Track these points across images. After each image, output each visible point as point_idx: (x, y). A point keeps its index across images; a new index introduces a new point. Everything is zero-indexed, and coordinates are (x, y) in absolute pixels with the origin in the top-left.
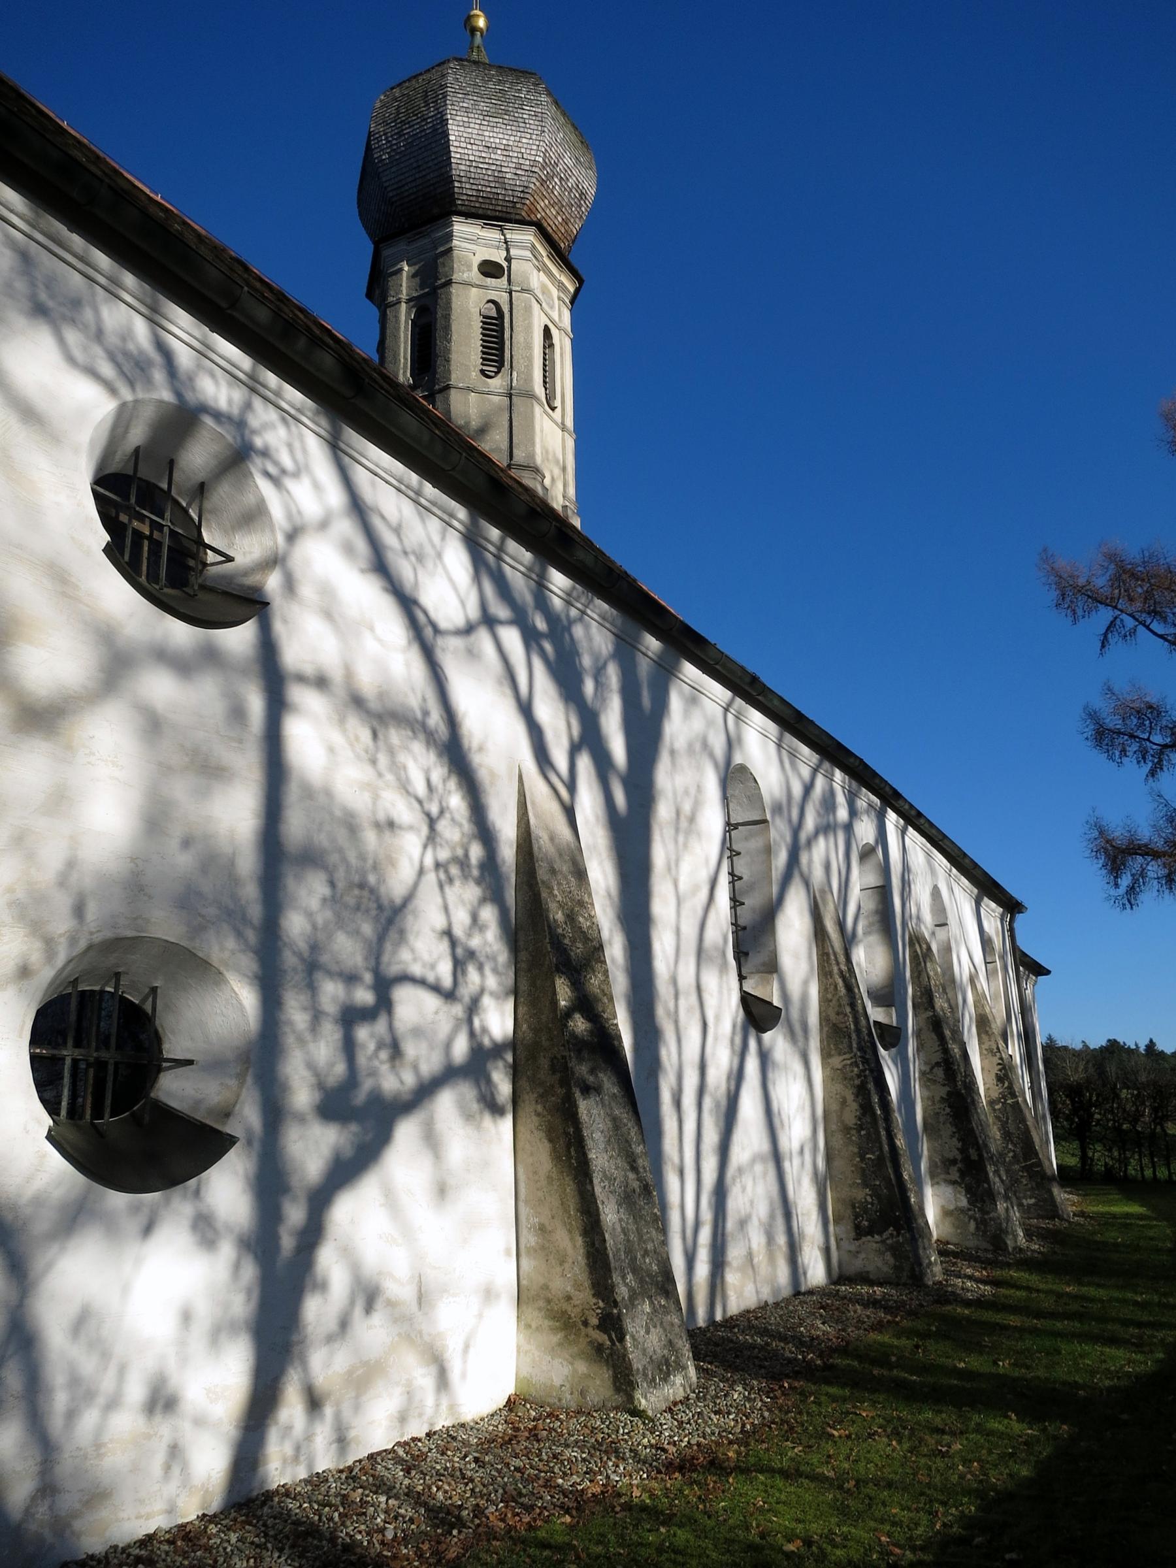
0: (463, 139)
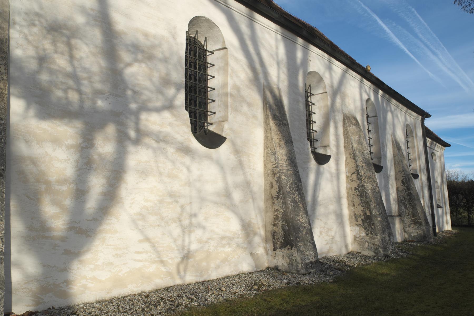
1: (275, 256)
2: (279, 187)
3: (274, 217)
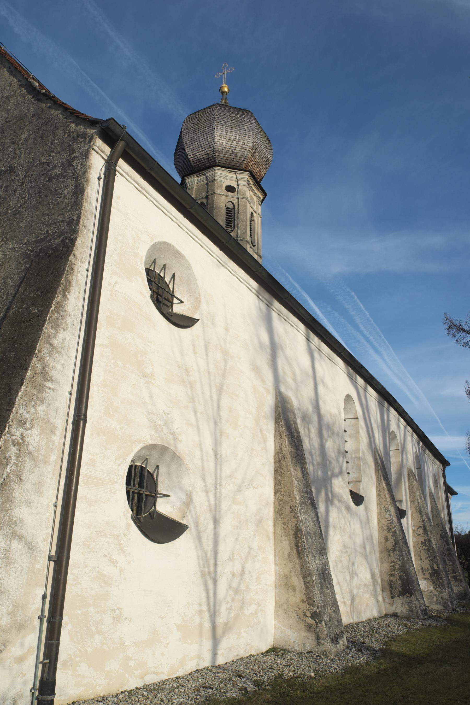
0: (220, 136)
1: (393, 604)
2: (395, 540)
3: (391, 567)
